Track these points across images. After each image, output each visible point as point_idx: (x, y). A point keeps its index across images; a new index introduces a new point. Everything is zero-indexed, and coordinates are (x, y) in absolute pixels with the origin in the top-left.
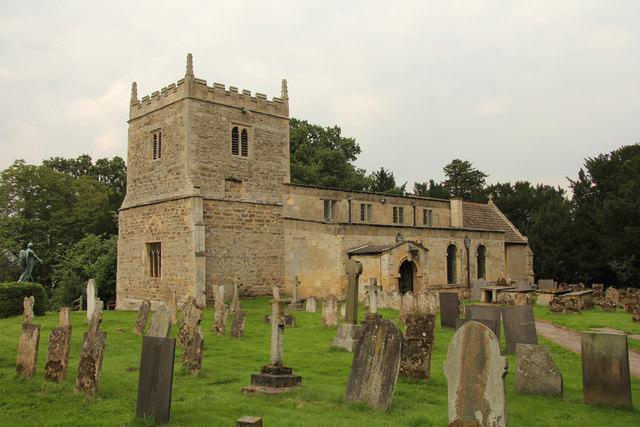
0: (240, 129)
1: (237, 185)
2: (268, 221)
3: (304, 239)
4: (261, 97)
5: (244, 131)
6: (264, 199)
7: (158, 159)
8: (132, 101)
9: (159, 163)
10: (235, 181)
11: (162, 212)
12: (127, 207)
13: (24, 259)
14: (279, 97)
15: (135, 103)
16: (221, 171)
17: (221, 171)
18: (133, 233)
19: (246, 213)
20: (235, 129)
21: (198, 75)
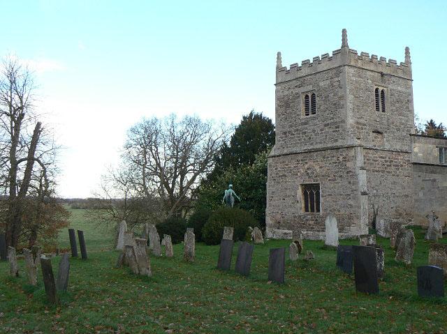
0: (380, 89)
1: (380, 136)
2: (402, 166)
3: (434, 180)
4: (392, 62)
5: (382, 91)
6: (398, 148)
7: (311, 115)
8: (277, 68)
9: (314, 118)
10: (378, 132)
11: (320, 158)
12: (277, 154)
13: (354, 175)
14: (404, 62)
15: (280, 70)
16: (370, 125)
17: (370, 125)
18: (285, 176)
19: (387, 159)
20: (377, 90)
21: (352, 45)
